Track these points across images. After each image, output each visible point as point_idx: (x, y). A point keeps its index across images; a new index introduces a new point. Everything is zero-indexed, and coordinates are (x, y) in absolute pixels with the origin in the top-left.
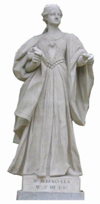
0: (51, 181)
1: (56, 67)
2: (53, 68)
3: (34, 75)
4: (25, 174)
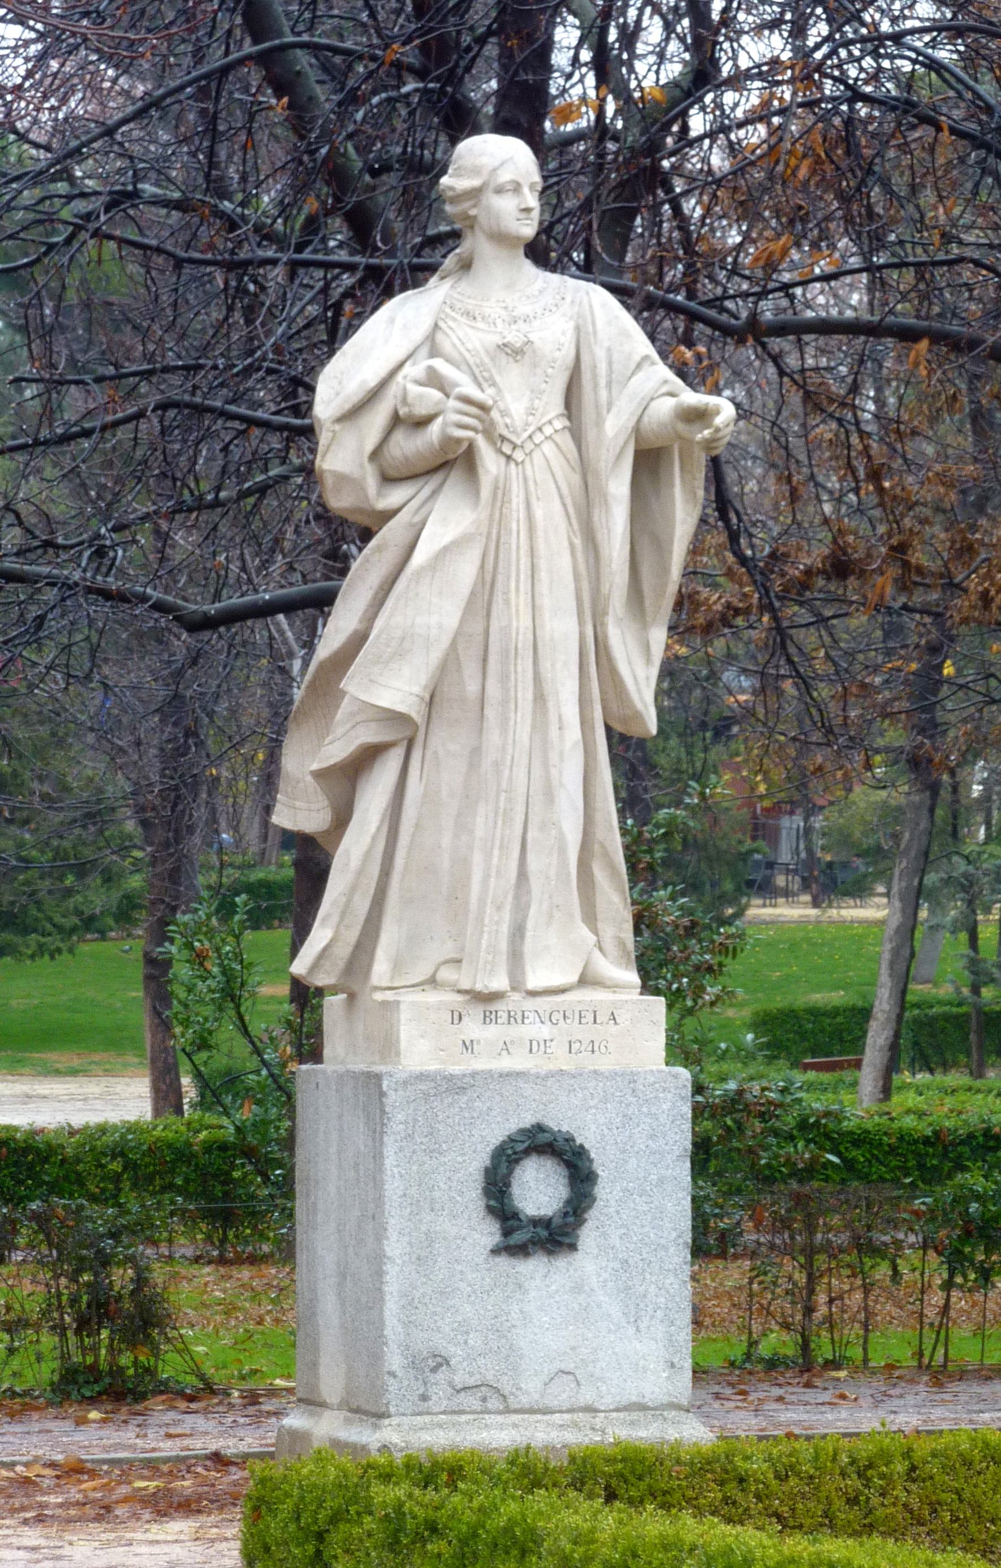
0: (531, 1016)
1: (537, 455)
3: (435, 493)
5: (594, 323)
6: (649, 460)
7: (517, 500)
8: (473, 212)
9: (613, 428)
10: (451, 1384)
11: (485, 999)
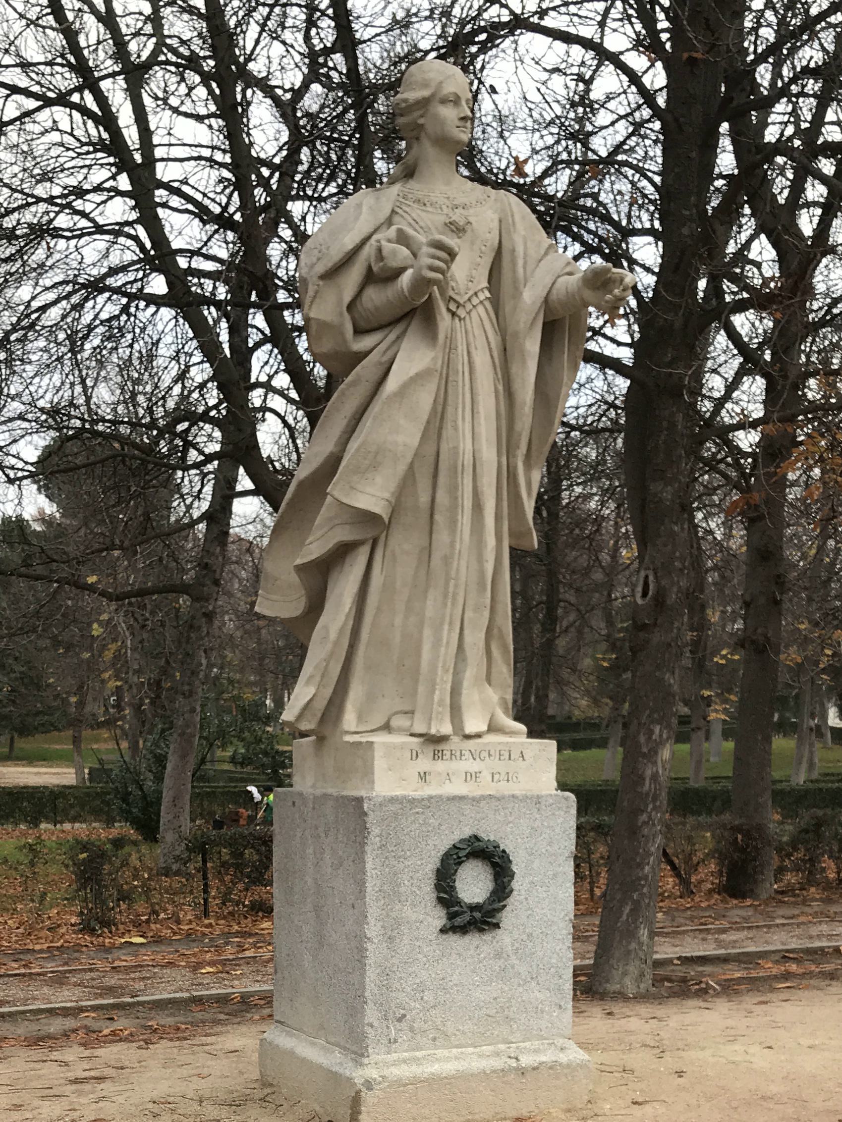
1: (474, 314)
3: (399, 338)
4: (353, 729)
5: (512, 216)
7: (462, 348)
8: (421, 121)
9: (531, 296)
11: (435, 741)
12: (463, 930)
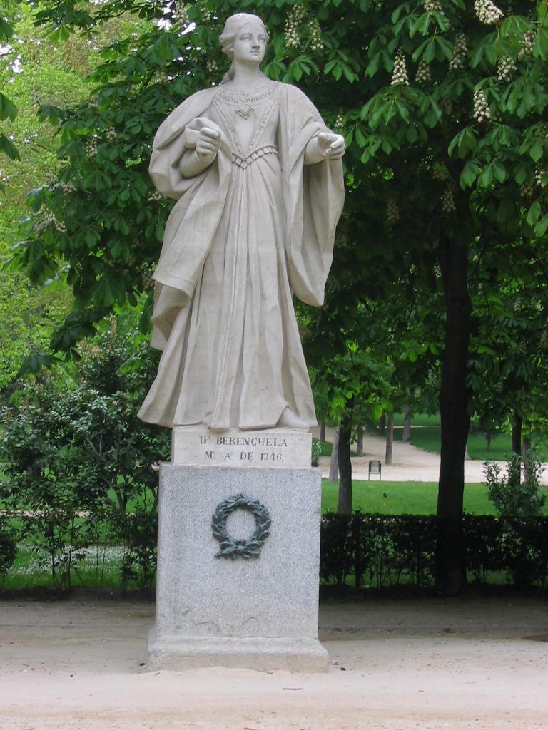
1: (254, 164)
2: (246, 168)
6: (312, 173)
8: (232, 50)
9: (293, 151)
10: (193, 621)
12: (226, 556)
